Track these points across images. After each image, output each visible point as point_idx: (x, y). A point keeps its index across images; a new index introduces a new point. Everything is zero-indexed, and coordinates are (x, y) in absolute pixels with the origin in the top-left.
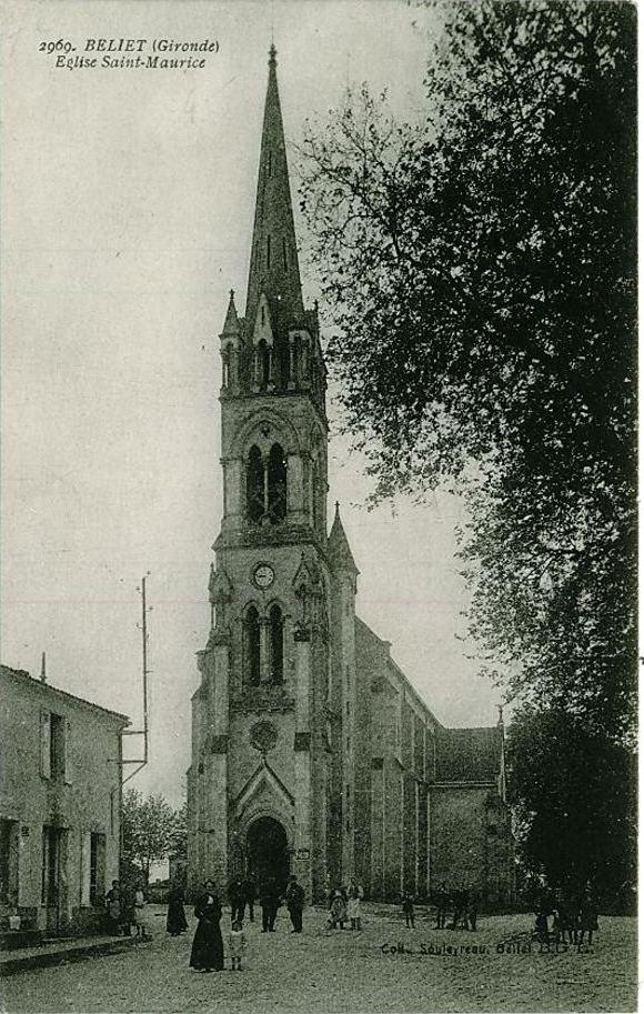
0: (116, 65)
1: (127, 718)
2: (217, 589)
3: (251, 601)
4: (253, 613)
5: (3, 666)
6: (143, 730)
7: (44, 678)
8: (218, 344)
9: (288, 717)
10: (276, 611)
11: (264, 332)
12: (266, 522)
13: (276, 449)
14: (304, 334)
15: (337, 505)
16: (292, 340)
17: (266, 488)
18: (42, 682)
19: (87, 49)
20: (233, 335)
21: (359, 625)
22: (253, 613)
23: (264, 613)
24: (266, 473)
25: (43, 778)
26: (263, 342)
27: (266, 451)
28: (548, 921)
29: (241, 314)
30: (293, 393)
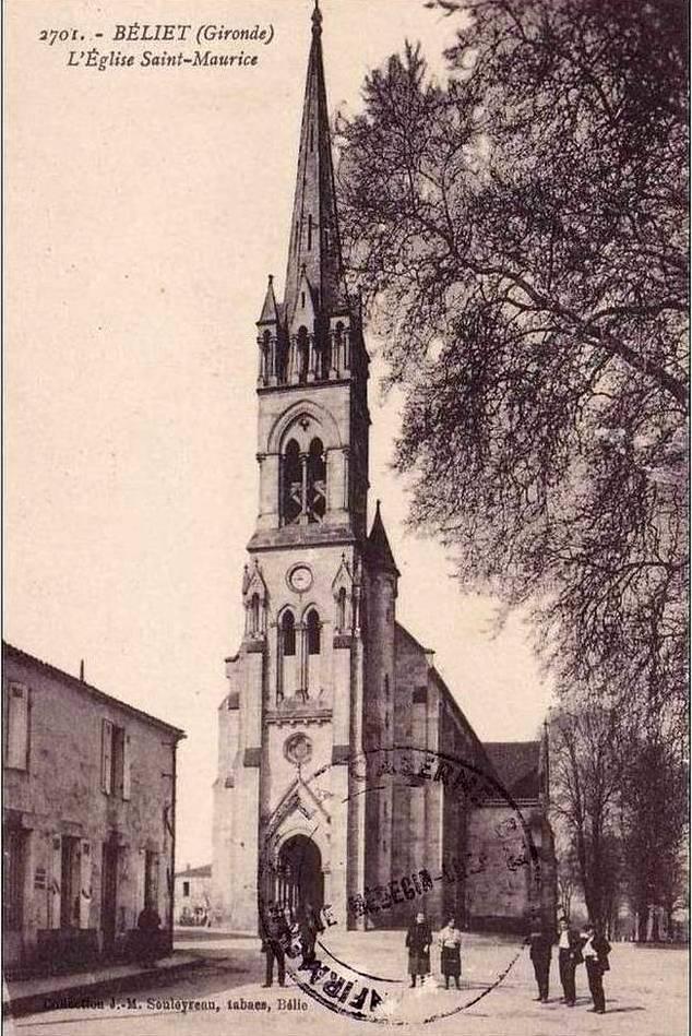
0: (157, 63)
1: (182, 731)
2: (250, 593)
3: (287, 605)
4: (289, 617)
5: (12, 654)
6: (309, 785)
7: (82, 676)
8: (255, 332)
9: (327, 726)
10: (314, 616)
11: (305, 318)
12: (304, 520)
13: (316, 444)
14: (346, 321)
15: (378, 503)
16: (333, 326)
17: (304, 485)
18: (82, 683)
19: (116, 39)
20: (269, 323)
21: (398, 629)
22: (289, 617)
23: (300, 618)
24: (305, 469)
25: (105, 794)
26: (303, 329)
27: (305, 447)
28: (553, 951)
29: (280, 299)
30: (332, 384)
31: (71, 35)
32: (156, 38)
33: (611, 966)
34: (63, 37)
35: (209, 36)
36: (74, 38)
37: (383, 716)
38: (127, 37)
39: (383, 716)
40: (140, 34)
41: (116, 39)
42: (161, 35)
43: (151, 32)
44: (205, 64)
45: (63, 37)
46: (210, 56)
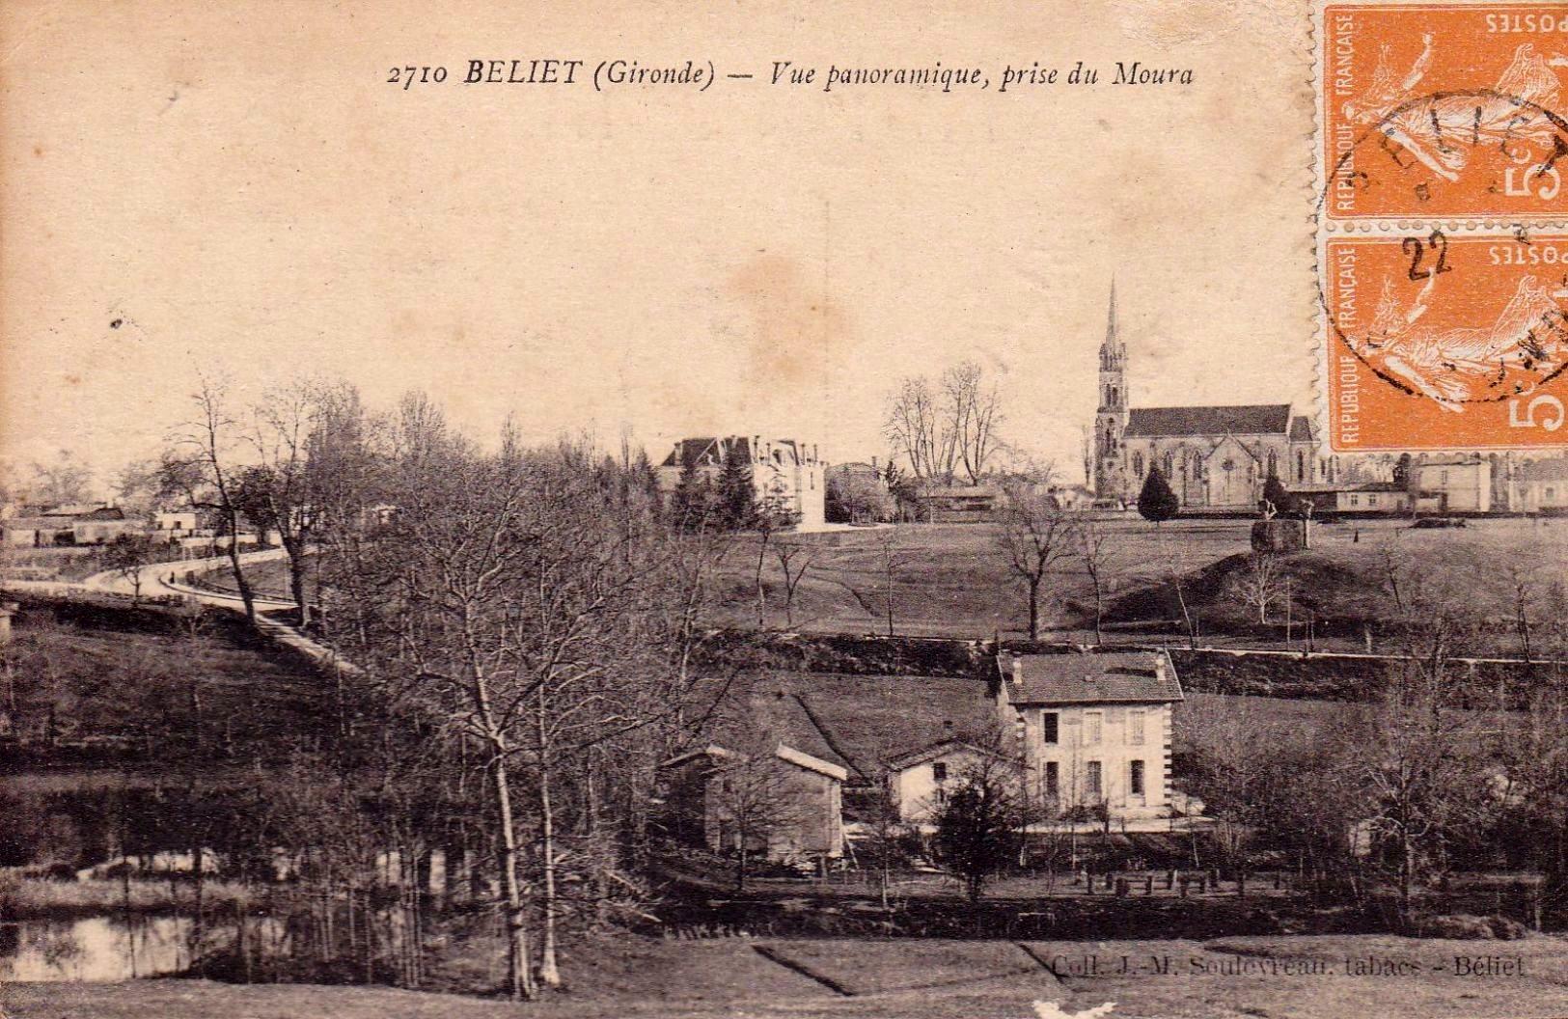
19: (469, 80)
31: (430, 74)
32: (531, 81)
33: (1059, 740)
34: (439, 77)
35: (616, 76)
36: (426, 70)
37: (1459, 917)
38: (485, 77)
39: (1459, 917)
40: (506, 75)
41: (469, 80)
42: (538, 76)
43: (523, 71)
44: (1132, 83)
45: (439, 77)
46: (1083, 70)
